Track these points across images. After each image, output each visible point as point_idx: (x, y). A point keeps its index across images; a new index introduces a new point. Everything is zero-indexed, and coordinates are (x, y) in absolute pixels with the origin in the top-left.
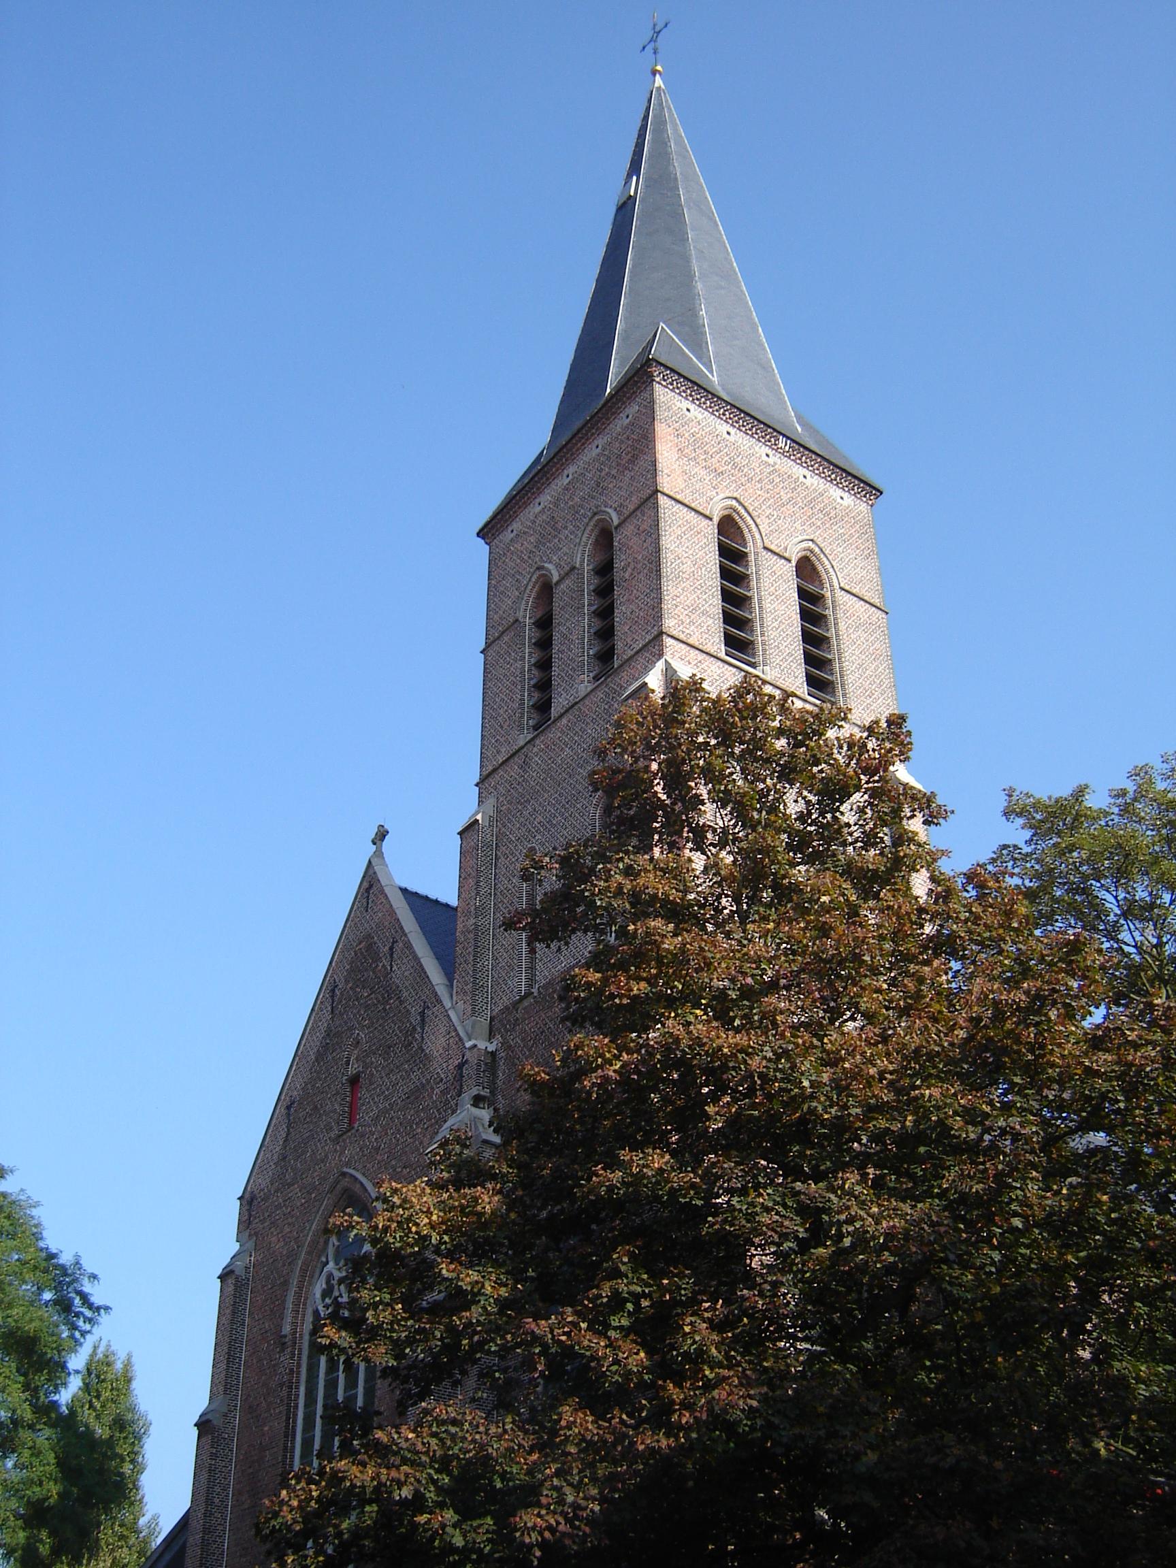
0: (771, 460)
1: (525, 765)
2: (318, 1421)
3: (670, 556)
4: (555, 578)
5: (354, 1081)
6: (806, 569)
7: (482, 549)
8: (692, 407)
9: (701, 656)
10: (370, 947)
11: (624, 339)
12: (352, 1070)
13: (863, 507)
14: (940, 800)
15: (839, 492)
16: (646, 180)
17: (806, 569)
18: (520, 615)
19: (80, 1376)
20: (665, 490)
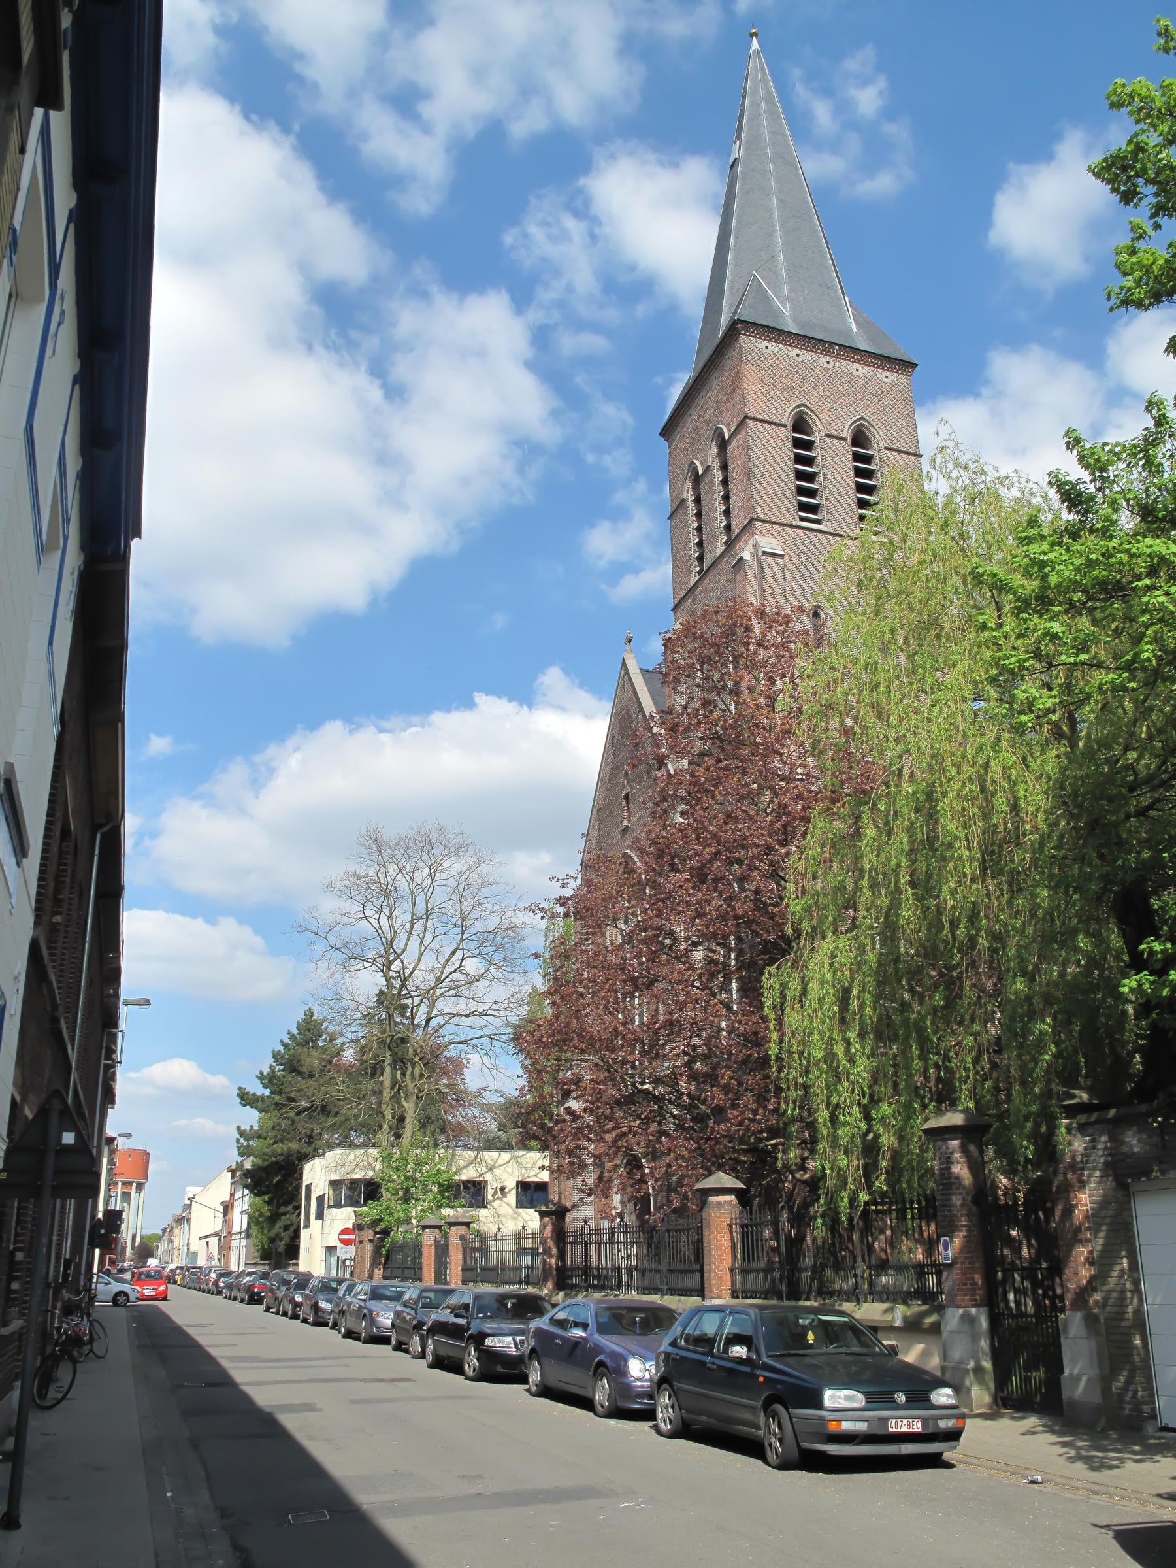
0: (831, 366)
1: (694, 600)
2: (83, 1271)
3: (757, 462)
4: (727, 436)
5: (627, 797)
6: (860, 438)
7: (663, 442)
8: (769, 344)
9: (780, 528)
10: (628, 713)
11: (732, 288)
12: (625, 790)
13: (903, 379)
14: (234, 1157)
15: (885, 373)
16: (746, 142)
17: (860, 438)
18: (684, 496)
19: (539, 962)
20: (752, 415)
